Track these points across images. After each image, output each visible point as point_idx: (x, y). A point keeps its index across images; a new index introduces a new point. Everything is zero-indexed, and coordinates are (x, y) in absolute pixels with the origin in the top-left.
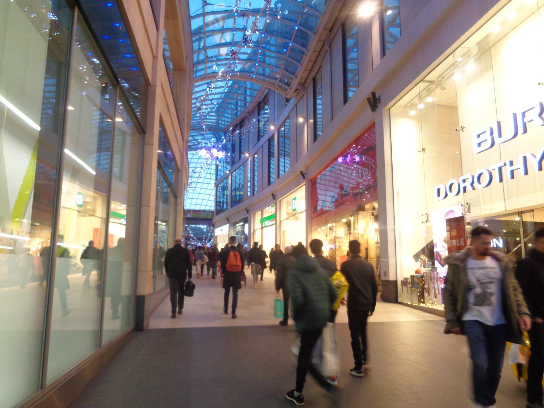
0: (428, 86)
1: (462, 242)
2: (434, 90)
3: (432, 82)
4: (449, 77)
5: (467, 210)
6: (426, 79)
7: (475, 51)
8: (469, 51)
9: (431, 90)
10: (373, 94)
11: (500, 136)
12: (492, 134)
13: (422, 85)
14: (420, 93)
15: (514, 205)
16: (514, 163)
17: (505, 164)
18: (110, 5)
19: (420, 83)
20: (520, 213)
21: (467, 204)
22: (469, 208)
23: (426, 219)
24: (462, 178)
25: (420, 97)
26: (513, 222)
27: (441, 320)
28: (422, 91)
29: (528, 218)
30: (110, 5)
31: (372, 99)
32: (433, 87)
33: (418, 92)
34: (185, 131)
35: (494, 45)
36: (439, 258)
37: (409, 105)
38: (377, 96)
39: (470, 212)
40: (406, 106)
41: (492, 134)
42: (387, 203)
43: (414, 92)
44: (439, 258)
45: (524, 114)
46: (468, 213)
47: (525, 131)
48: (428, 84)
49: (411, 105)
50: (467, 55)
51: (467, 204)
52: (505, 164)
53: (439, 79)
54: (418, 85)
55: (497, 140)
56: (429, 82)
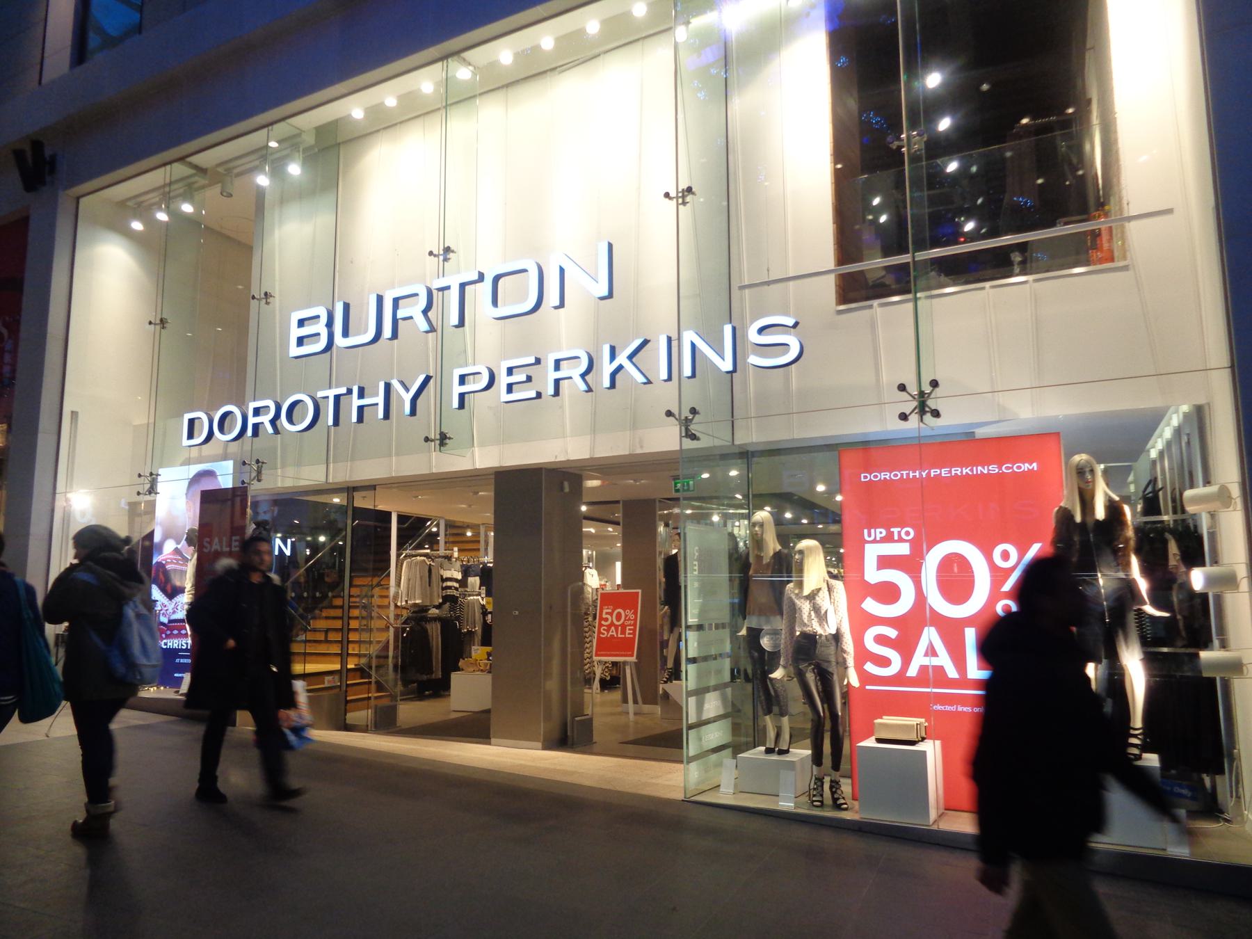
0: (191, 176)
1: (234, 544)
2: (203, 187)
3: (201, 170)
4: (239, 175)
5: (254, 474)
6: (189, 159)
7: (309, 139)
8: (299, 135)
9: (196, 186)
10: (37, 145)
11: (346, 334)
12: (330, 324)
13: (179, 170)
14: (170, 184)
15: (343, 473)
16: (366, 391)
17: (350, 392)
18: (980, 201)
19: (175, 165)
20: (351, 490)
21: (258, 461)
22: (259, 472)
23: (147, 486)
24: (252, 405)
25: (167, 196)
26: (325, 505)
27: (166, 722)
28: (177, 181)
29: (361, 502)
30: (980, 201)
31: (29, 154)
32: (201, 181)
33: (168, 181)
34: (1166, 432)
35: (345, 142)
36: (161, 576)
37: (130, 204)
38: (48, 152)
39: (259, 480)
40: (122, 204)
41: (330, 324)
42: (40, 436)
43: (156, 178)
44: (161, 576)
45: (396, 301)
46: (255, 482)
47: (395, 335)
48: (191, 171)
49: (140, 208)
50: (291, 143)
51: (258, 461)
52: (350, 392)
53: (220, 170)
54: (168, 167)
55: (340, 341)
56: (196, 167)
